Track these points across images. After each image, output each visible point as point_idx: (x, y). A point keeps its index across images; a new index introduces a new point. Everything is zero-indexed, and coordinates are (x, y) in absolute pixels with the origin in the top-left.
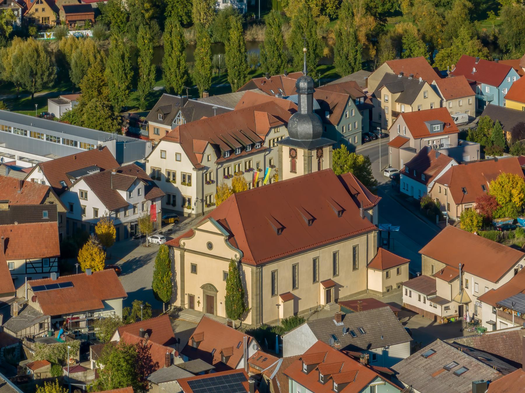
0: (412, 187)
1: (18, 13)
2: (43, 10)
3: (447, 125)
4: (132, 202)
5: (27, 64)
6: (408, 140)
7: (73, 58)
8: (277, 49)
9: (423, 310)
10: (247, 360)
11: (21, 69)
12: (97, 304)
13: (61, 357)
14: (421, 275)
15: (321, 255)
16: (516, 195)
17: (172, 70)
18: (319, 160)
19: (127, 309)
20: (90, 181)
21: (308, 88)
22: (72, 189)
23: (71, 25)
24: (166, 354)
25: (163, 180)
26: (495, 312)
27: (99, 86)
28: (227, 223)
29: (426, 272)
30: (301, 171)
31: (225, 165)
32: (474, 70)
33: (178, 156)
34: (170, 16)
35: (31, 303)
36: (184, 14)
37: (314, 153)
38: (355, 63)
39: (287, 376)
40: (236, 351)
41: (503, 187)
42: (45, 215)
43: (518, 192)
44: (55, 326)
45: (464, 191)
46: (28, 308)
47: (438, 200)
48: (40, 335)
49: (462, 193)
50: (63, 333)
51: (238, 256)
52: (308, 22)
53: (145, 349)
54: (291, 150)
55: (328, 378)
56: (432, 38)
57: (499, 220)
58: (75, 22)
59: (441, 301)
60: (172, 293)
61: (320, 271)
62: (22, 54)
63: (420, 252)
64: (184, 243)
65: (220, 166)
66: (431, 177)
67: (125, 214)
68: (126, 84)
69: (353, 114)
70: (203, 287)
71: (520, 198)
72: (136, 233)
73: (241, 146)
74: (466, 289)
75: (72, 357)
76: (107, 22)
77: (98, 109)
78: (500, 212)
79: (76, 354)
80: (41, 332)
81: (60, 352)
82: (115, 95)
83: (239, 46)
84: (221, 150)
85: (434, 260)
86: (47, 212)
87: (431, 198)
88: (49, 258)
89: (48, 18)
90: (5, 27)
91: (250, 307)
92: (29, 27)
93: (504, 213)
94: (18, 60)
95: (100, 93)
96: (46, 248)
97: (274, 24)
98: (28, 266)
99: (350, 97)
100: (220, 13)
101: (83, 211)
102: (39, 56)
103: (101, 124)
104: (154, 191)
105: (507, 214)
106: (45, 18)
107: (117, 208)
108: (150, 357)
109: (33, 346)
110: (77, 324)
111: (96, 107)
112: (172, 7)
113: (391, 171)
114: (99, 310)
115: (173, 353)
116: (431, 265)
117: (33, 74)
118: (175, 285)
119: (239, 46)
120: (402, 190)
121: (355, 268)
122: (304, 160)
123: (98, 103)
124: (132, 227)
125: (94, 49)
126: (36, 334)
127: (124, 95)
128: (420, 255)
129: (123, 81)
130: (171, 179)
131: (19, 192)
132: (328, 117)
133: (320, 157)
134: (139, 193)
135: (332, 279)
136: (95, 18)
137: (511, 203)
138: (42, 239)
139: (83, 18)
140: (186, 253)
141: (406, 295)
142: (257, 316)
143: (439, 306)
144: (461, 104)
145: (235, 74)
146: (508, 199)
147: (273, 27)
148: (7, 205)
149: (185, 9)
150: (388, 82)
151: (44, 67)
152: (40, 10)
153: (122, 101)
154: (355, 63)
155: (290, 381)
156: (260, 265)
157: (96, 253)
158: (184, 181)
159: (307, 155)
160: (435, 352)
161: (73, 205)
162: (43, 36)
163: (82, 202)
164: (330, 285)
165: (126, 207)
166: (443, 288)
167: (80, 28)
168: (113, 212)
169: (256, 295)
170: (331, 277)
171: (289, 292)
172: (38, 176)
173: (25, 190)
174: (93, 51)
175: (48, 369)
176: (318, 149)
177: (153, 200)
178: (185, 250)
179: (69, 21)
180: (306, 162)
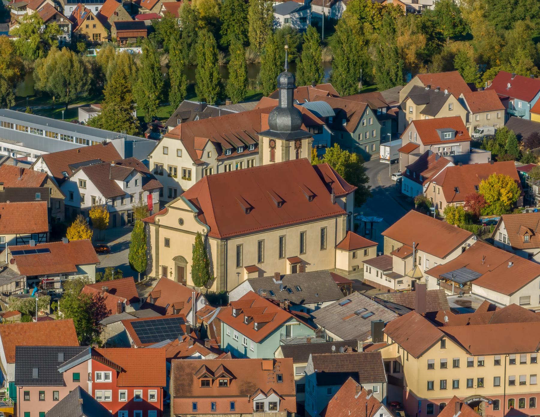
0: (412, 188)
1: (68, 28)
2: (94, 26)
3: (459, 133)
4: (129, 191)
5: (60, 74)
6: (418, 146)
7: (108, 69)
8: (314, 63)
9: (380, 285)
10: (196, 313)
11: (55, 78)
12: (71, 268)
13: (32, 310)
14: (383, 254)
15: (288, 234)
16: (504, 194)
17: (205, 82)
18: (297, 151)
19: (100, 274)
20: (88, 172)
21: (288, 84)
22: (72, 179)
23: (122, 42)
24: (118, 303)
25: (165, 175)
26: (439, 284)
27: (123, 93)
28: (198, 202)
29: (387, 252)
30: (279, 159)
31: (226, 162)
32: (509, 85)
33: (179, 152)
34: (226, 34)
35: (10, 266)
36: (240, 33)
37: (292, 144)
38: (396, 79)
39: (219, 320)
40: (186, 306)
41: (492, 186)
42: (38, 196)
43: (506, 191)
44: (30, 286)
45: (456, 190)
46: (8, 270)
47: (432, 198)
48: (16, 292)
49: (455, 192)
50: (37, 291)
51: (206, 231)
52: (348, 36)
53: (101, 299)
54: (270, 141)
55: (251, 319)
56: (489, 58)
57: (486, 217)
58: (126, 39)
59: (395, 276)
60: (147, 264)
61: (286, 249)
62: (56, 63)
63: (382, 234)
64: (159, 220)
65: (221, 163)
66: (427, 178)
67: (122, 202)
68: (157, 94)
69: (371, 123)
70: (175, 259)
71: (508, 197)
72: (133, 221)
73: (244, 145)
74: (419, 266)
75: (43, 310)
76: (160, 39)
77: (116, 112)
78: (488, 210)
79: (47, 308)
80: (17, 289)
81: (31, 305)
82: (146, 105)
83: (275, 59)
84: (223, 148)
85: (394, 241)
86: (39, 194)
87: (426, 197)
88: (38, 233)
89: (100, 34)
90: (50, 41)
91: (215, 276)
92: (78, 44)
93: (492, 211)
94: (51, 69)
95: (123, 99)
96: (36, 224)
97: (312, 38)
98: (18, 240)
99: (368, 105)
100: (277, 32)
101: (82, 200)
102: (72, 66)
103: (118, 127)
104: (152, 183)
105: (495, 212)
106: (97, 35)
107: (113, 196)
108: (105, 306)
109: (7, 300)
110: (52, 284)
111: (114, 110)
112: (228, 26)
113: (398, 175)
114: (72, 274)
115: (125, 302)
116: (391, 244)
117: (66, 84)
118: (151, 256)
119: (275, 59)
120: (403, 192)
121: (322, 247)
122: (282, 150)
123: (116, 107)
124: (129, 215)
125: (129, 61)
126: (12, 291)
127: (155, 105)
128: (383, 236)
129: (153, 91)
130: (173, 174)
131: (19, 179)
132: (345, 124)
133: (298, 148)
134: (136, 184)
135: (299, 256)
136: (148, 35)
137: (499, 202)
138: (34, 216)
139: (136, 35)
140: (160, 229)
141: (367, 271)
142: (221, 284)
143: (393, 280)
144: (489, 118)
145: (270, 87)
146: (496, 197)
147: (311, 41)
148: (2, 186)
149: (242, 28)
150: (418, 96)
151: (78, 78)
152: (91, 26)
153: (153, 111)
154: (396, 79)
155: (222, 324)
156: (225, 238)
157: (83, 231)
158: (185, 176)
159: (284, 145)
160: (351, 301)
161: (73, 194)
162: (92, 53)
163: (81, 191)
164: (296, 262)
165: (123, 196)
166: (398, 265)
167: (131, 45)
168: (109, 200)
169: (221, 265)
170: (298, 254)
171: (254, 265)
172: (40, 166)
173: (25, 177)
174: (128, 62)
175: (18, 317)
176: (296, 140)
177: (151, 191)
178: (160, 226)
179: (120, 38)
180: (284, 152)
